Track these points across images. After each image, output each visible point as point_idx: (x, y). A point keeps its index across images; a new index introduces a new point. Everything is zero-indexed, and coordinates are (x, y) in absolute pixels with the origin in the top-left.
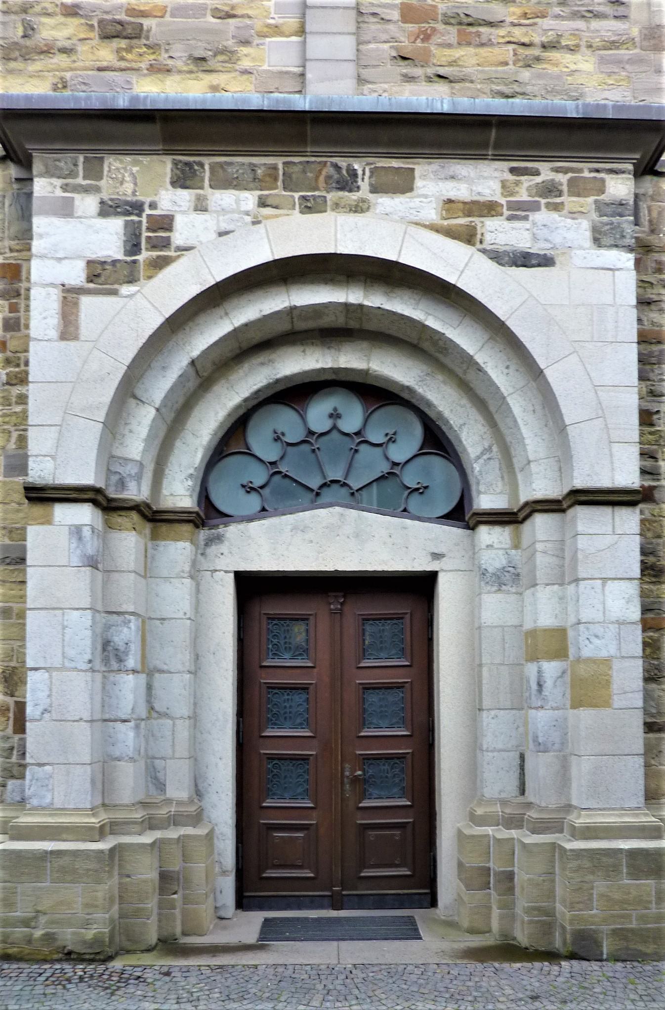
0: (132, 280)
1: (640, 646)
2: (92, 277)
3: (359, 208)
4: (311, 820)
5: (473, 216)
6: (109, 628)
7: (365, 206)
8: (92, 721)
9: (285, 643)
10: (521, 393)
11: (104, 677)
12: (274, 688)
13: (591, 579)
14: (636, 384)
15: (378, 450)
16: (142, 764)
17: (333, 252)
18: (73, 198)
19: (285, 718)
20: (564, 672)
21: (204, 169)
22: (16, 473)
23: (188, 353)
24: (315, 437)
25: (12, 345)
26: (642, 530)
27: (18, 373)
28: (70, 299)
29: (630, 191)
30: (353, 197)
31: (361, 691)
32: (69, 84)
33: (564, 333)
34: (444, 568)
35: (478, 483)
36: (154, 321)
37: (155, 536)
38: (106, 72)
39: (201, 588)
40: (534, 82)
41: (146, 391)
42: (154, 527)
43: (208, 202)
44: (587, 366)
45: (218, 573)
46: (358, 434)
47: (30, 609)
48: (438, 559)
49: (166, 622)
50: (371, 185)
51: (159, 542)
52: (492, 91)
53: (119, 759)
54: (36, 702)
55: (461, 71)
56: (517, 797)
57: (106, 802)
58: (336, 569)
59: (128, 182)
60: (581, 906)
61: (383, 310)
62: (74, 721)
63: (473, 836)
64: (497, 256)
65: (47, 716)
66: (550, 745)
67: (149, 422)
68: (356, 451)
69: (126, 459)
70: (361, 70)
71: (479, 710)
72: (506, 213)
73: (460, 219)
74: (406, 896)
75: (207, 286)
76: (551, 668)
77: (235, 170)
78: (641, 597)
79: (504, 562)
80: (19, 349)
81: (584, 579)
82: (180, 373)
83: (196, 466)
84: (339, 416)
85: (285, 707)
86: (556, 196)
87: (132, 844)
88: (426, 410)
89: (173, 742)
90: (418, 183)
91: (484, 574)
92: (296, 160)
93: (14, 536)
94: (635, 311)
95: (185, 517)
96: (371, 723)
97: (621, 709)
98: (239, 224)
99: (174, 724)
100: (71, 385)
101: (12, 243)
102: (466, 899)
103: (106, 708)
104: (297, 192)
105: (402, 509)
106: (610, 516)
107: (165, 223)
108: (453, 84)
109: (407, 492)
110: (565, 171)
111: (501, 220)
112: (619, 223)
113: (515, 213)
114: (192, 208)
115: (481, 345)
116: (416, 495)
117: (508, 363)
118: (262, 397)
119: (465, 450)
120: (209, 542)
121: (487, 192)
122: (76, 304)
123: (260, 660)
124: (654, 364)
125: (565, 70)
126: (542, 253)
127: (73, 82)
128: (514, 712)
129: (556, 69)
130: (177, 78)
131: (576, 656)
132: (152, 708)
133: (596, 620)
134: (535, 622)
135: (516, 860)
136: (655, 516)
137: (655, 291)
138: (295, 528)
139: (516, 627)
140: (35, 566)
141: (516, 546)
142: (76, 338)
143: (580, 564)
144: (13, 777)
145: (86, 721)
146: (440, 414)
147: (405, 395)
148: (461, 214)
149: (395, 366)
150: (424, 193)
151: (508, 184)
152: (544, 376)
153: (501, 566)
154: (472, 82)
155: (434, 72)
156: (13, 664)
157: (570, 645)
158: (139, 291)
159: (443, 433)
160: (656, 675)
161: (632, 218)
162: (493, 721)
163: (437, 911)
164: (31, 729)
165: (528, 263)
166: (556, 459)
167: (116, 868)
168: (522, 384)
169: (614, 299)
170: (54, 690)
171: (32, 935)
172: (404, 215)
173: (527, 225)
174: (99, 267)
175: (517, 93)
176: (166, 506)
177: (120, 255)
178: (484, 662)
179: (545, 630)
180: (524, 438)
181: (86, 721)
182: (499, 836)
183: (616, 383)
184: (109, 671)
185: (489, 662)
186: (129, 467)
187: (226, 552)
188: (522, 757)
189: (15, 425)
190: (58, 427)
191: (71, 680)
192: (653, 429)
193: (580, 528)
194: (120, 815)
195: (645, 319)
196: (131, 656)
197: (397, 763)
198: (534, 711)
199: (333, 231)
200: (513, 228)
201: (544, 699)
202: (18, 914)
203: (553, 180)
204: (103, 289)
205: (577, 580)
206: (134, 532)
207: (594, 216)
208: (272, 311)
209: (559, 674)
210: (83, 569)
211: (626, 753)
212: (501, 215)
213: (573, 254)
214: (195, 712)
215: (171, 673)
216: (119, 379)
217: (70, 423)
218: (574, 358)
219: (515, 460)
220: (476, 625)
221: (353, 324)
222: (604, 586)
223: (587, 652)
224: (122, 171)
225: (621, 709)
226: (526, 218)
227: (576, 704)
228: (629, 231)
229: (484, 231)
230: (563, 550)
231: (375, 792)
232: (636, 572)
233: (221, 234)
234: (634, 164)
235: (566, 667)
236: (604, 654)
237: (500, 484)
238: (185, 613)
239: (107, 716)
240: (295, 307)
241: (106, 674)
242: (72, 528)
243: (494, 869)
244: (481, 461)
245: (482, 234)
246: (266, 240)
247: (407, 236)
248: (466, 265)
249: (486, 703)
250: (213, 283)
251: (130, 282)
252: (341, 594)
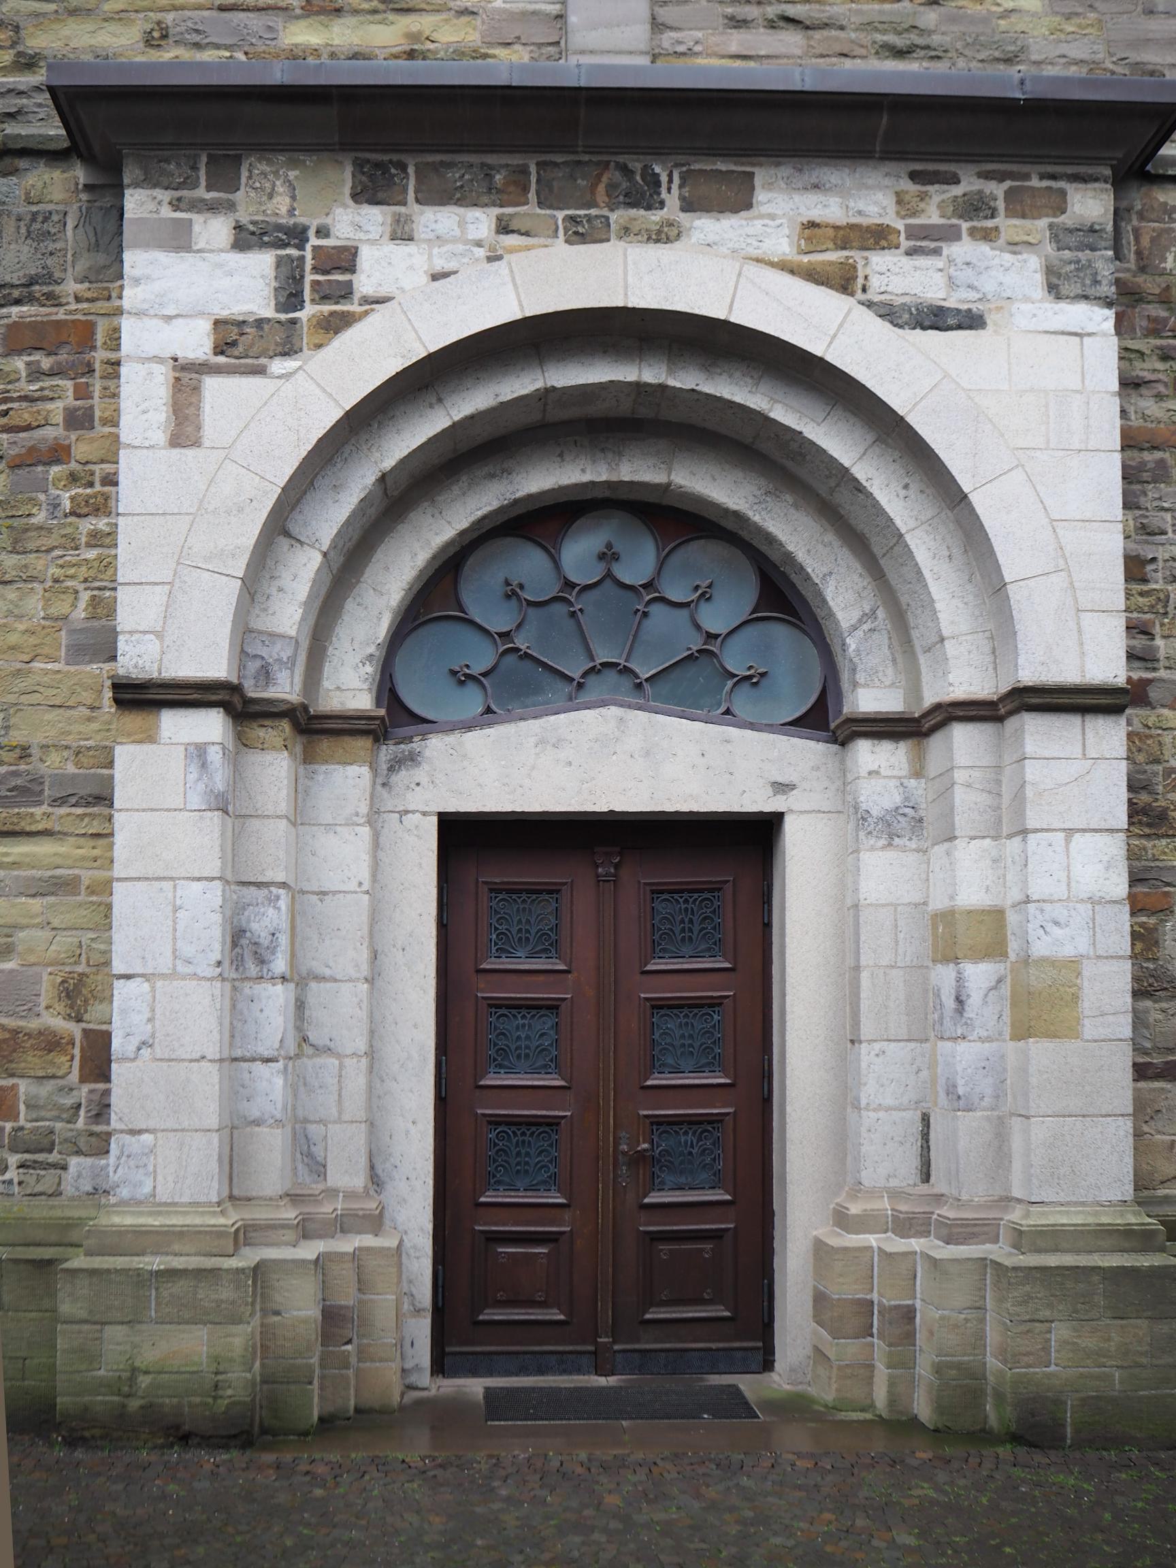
0: (289, 351)
1: (1129, 938)
2: (220, 348)
3: (663, 235)
4: (560, 1225)
5: (852, 248)
6: (244, 909)
7: (673, 232)
8: (221, 1060)
9: (520, 930)
10: (929, 529)
11: (234, 988)
12: (499, 1007)
13: (1047, 830)
14: (1120, 518)
15: (684, 613)
16: (289, 1128)
17: (621, 304)
18: (191, 220)
19: (519, 1057)
20: (999, 981)
21: (407, 173)
22: (87, 658)
23: (376, 463)
24: (574, 593)
25: (82, 450)
26: (1129, 750)
27: (89, 496)
28: (185, 381)
29: (1106, 211)
30: (653, 218)
31: (649, 1012)
32: (171, 31)
33: (1003, 435)
34: (794, 808)
35: (854, 670)
36: (327, 416)
37: (309, 758)
38: (236, 13)
39: (382, 840)
40: (943, 29)
41: (305, 524)
42: (309, 742)
43: (414, 226)
44: (1038, 488)
45: (410, 815)
46: (648, 586)
47: (119, 880)
48: (784, 793)
49: (328, 898)
50: (682, 198)
51: (316, 767)
52: (875, 42)
53: (257, 1123)
54: (128, 1030)
55: (824, 11)
56: (915, 1185)
57: (236, 1192)
58: (611, 808)
59: (281, 195)
60: (1030, 1359)
61: (700, 393)
62: (191, 1061)
63: (846, 1249)
64: (890, 313)
65: (146, 1052)
66: (976, 1101)
67: (312, 575)
68: (645, 614)
69: (272, 635)
70: (657, 9)
71: (852, 1042)
72: (905, 244)
73: (828, 253)
74: (721, 1353)
75: (414, 360)
76: (979, 974)
77: (457, 175)
78: (1129, 859)
79: (898, 799)
80: (90, 458)
81: (1036, 831)
82: (362, 496)
83: (379, 641)
84: (616, 557)
85: (519, 1038)
86: (986, 218)
87: (285, 1261)
88: (764, 548)
89: (340, 1095)
90: (760, 196)
91: (864, 819)
92: (559, 159)
93: (83, 759)
94: (1117, 400)
95: (362, 725)
96: (663, 1065)
97: (1096, 1041)
98: (466, 260)
99: (341, 1067)
100: (191, 517)
101: (79, 286)
102: (831, 1353)
103: (238, 1039)
104: (562, 209)
105: (722, 709)
106: (1078, 730)
108: (810, 32)
109: (730, 683)
110: (1001, 177)
111: (895, 255)
112: (1089, 261)
113: (919, 244)
114: (387, 236)
115: (862, 451)
116: (745, 687)
117: (907, 480)
118: (488, 525)
119: (831, 614)
120: (396, 765)
121: (873, 209)
122: (196, 389)
123: (477, 961)
124: (1148, 482)
125: (994, 8)
126: (964, 307)
127: (178, 29)
128: (913, 1045)
129: (979, 7)
130: (351, 21)
131: (1022, 954)
132: (305, 1039)
133: (1056, 897)
134: (952, 898)
135: (918, 1288)
136: (1149, 728)
137: (1147, 365)
138: (542, 742)
139: (916, 905)
140: (127, 810)
141: (918, 773)
142: (196, 443)
143: (1028, 805)
144: (78, 1153)
145: (210, 1061)
146: (789, 558)
147: (729, 524)
148: (831, 245)
149: (714, 479)
150: (770, 211)
151: (907, 198)
152: (970, 504)
153: (893, 806)
154: (842, 28)
155: (779, 12)
156: (80, 969)
157: (1010, 937)
158: (300, 368)
159: (793, 586)
160: (1151, 985)
161: (1110, 253)
162: (879, 1060)
163: (774, 1376)
164: (119, 1075)
165: (940, 324)
166: (988, 634)
167: (258, 1300)
168: (930, 514)
169: (1083, 382)
170: (158, 1011)
171: (124, 1406)
172: (737, 246)
173: (939, 263)
174: (236, 330)
175: (917, 46)
176: (328, 708)
177: (268, 311)
178: (863, 962)
179: (970, 912)
180: (933, 601)
181: (210, 1061)
182: (889, 1248)
183: (1088, 516)
184: (243, 980)
185: (871, 963)
186: (278, 646)
187: (424, 781)
188: (926, 1119)
189: (86, 580)
190: (168, 587)
191: (187, 995)
192: (1145, 588)
193: (1030, 748)
194: (260, 1214)
195: (1131, 410)
196: (279, 955)
197: (708, 1131)
198: (949, 1044)
199: (620, 271)
200: (916, 269)
201: (966, 1024)
202: (102, 1372)
203: (980, 192)
204: (240, 366)
205: (1024, 832)
206: (286, 753)
207: (1049, 249)
208: (515, 395)
209: (993, 984)
210: (209, 814)
211: (1104, 1112)
212: (897, 247)
213: (1014, 310)
214: (372, 1046)
215: (336, 980)
216: (269, 509)
217: (186, 579)
218: (1018, 475)
219: (915, 634)
220: (849, 902)
221: (644, 412)
222: (1068, 841)
223: (1041, 948)
224: (271, 177)
225: (1096, 1041)
226: (937, 252)
227: (1022, 1032)
228: (1107, 273)
229: (868, 271)
230: (998, 782)
231: (670, 1179)
232: (1122, 820)
233: (435, 277)
234: (1112, 166)
235: (1003, 972)
236: (1068, 951)
237: (890, 671)
238: (360, 884)
239: (238, 1053)
240: (554, 388)
241: (237, 984)
242: (191, 749)
243: (880, 1303)
244: (859, 633)
245: (866, 277)
246: (510, 286)
247: (743, 280)
248: (841, 326)
249: (867, 1030)
250: (424, 354)
251: (285, 354)
252: (618, 849)
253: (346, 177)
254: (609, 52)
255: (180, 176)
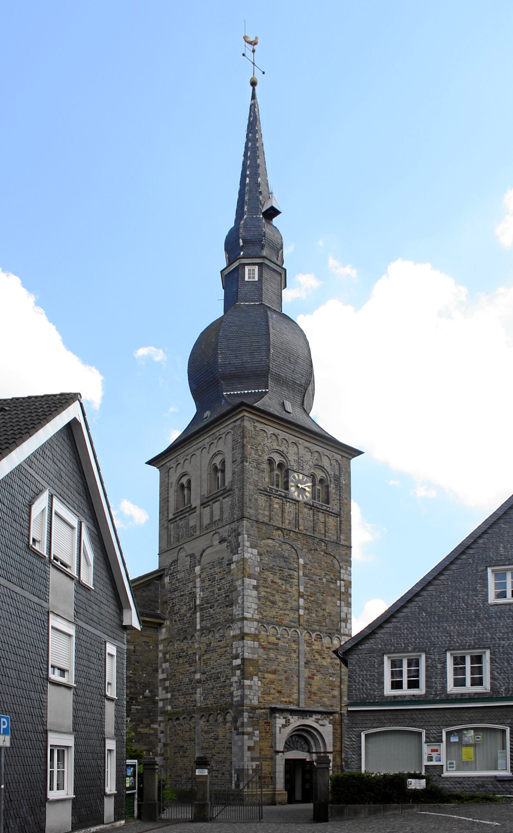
0: (286, 727)
3: (308, 719)
107: (289, 720)
253: (289, 714)
254: (86, 559)
255: (223, 677)
